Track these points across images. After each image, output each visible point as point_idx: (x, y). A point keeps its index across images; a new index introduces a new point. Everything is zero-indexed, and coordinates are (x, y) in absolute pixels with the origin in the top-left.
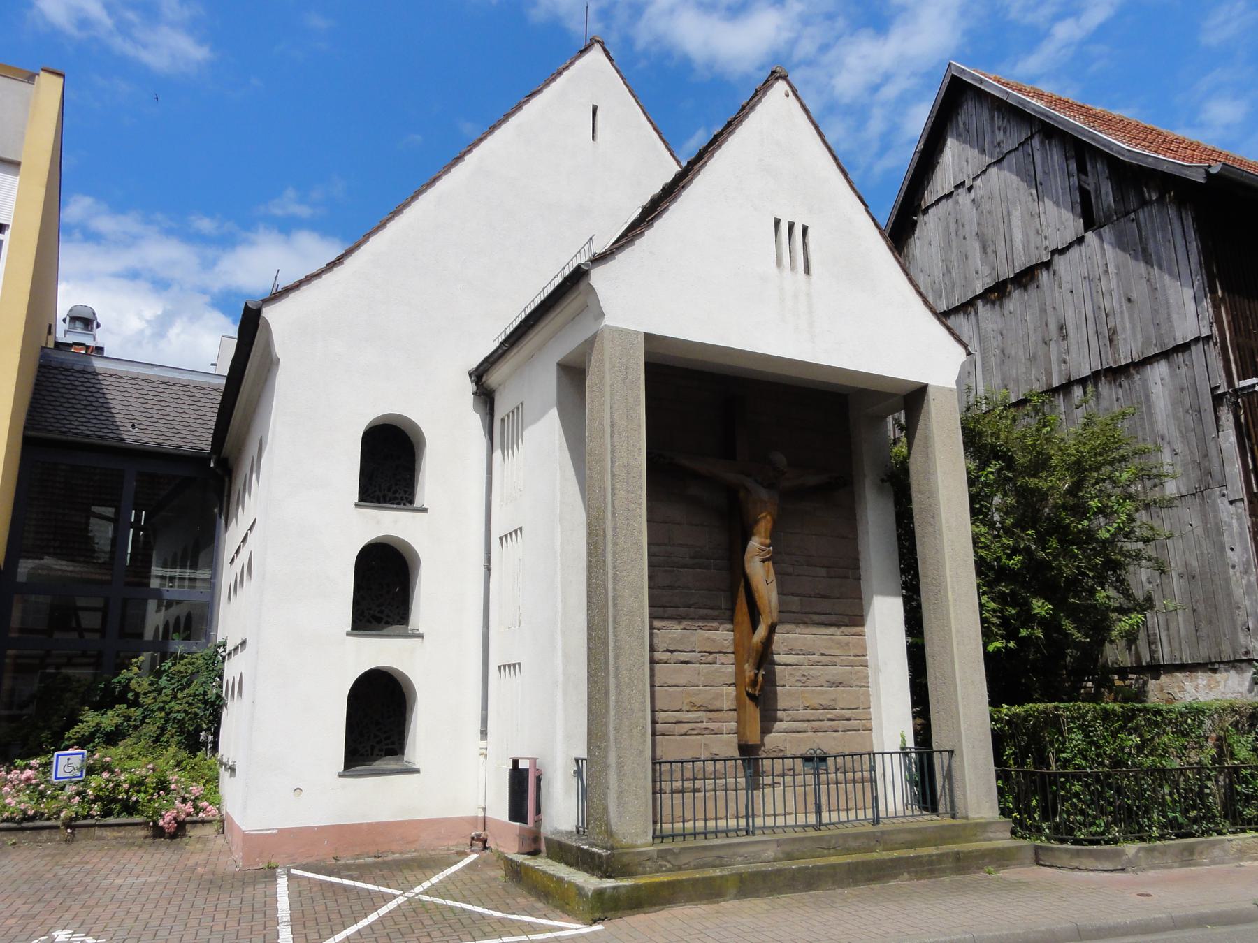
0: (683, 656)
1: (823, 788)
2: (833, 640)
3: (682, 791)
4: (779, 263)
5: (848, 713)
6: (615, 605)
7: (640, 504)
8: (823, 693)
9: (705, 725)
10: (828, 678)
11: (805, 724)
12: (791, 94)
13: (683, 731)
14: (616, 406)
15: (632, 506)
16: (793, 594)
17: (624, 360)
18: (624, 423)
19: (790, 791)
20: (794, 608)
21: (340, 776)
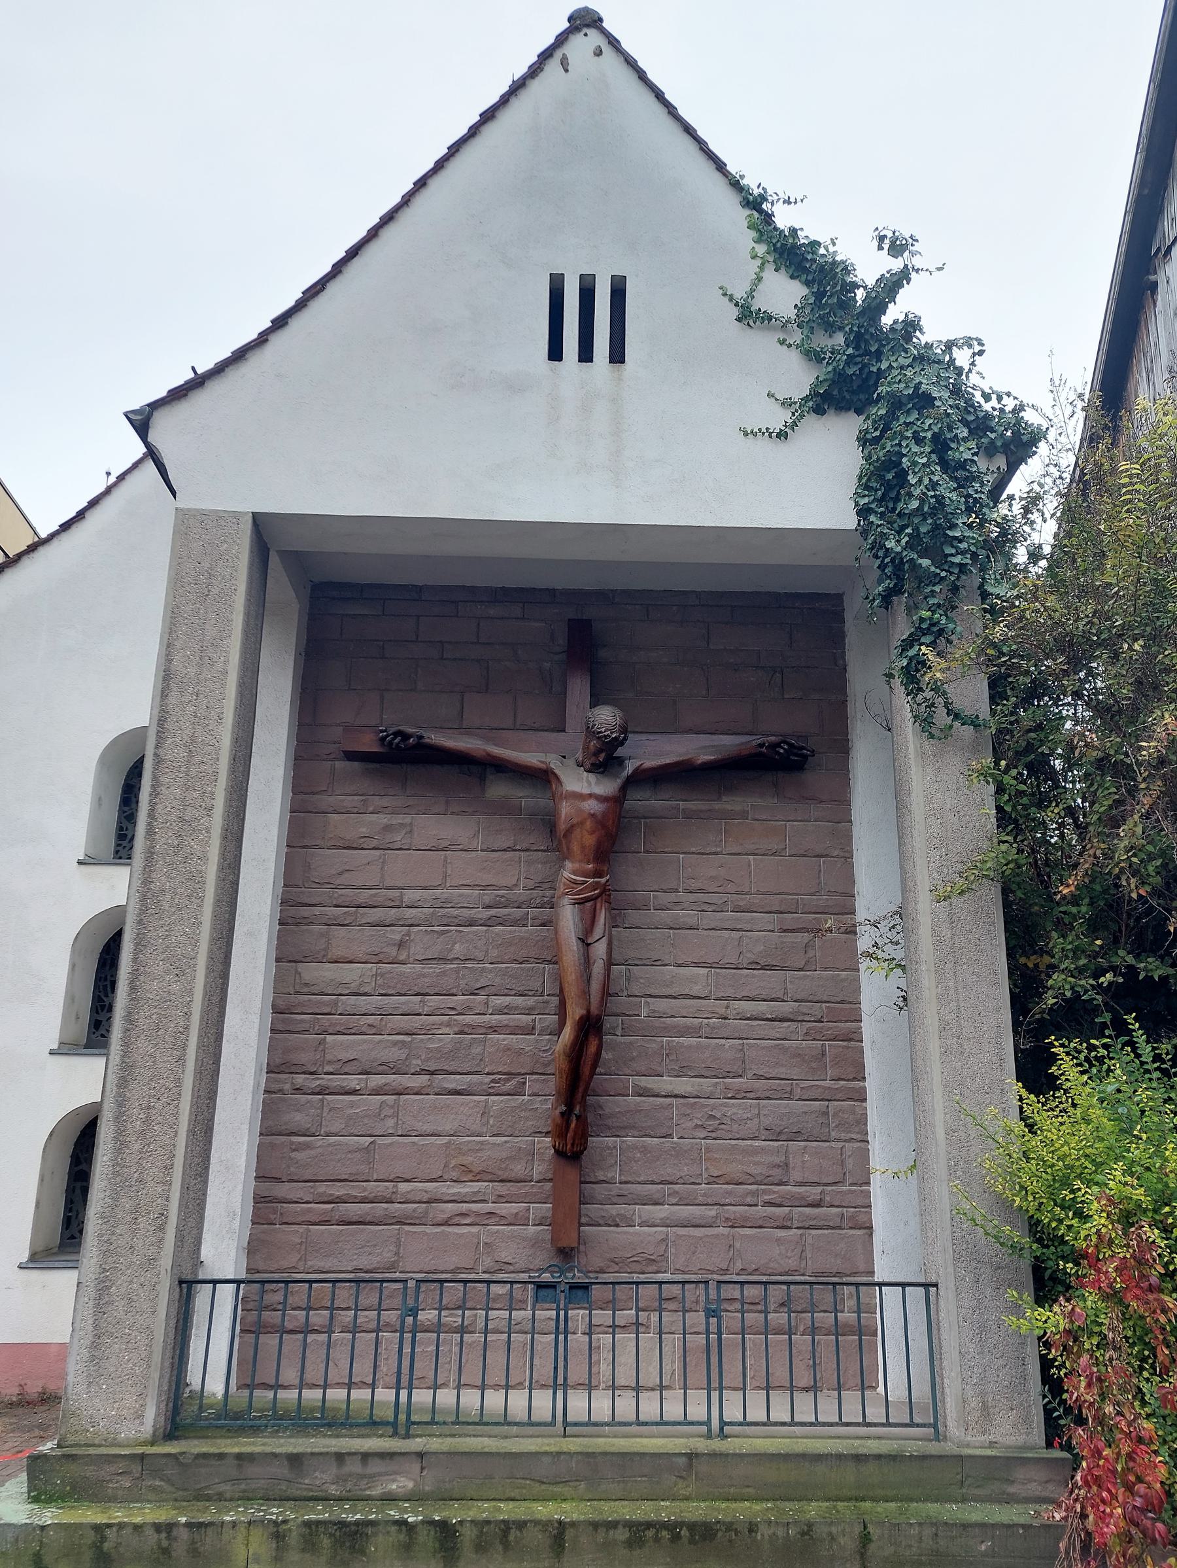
0: (452, 1082)
1: (578, 1340)
2: (784, 1050)
3: (438, 1328)
4: (555, 352)
5: (339, 1190)
6: (133, 988)
7: (210, 809)
8: (756, 1151)
9: (489, 1207)
10: (766, 1122)
11: (712, 1212)
12: (606, 49)
13: (442, 1217)
14: (178, 644)
15: (191, 813)
16: (697, 965)
17: (206, 565)
18: (193, 670)
19: (673, 1342)
20: (696, 990)
21: (21, 1267)
